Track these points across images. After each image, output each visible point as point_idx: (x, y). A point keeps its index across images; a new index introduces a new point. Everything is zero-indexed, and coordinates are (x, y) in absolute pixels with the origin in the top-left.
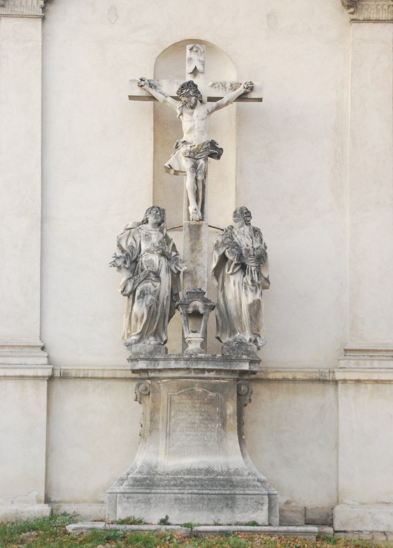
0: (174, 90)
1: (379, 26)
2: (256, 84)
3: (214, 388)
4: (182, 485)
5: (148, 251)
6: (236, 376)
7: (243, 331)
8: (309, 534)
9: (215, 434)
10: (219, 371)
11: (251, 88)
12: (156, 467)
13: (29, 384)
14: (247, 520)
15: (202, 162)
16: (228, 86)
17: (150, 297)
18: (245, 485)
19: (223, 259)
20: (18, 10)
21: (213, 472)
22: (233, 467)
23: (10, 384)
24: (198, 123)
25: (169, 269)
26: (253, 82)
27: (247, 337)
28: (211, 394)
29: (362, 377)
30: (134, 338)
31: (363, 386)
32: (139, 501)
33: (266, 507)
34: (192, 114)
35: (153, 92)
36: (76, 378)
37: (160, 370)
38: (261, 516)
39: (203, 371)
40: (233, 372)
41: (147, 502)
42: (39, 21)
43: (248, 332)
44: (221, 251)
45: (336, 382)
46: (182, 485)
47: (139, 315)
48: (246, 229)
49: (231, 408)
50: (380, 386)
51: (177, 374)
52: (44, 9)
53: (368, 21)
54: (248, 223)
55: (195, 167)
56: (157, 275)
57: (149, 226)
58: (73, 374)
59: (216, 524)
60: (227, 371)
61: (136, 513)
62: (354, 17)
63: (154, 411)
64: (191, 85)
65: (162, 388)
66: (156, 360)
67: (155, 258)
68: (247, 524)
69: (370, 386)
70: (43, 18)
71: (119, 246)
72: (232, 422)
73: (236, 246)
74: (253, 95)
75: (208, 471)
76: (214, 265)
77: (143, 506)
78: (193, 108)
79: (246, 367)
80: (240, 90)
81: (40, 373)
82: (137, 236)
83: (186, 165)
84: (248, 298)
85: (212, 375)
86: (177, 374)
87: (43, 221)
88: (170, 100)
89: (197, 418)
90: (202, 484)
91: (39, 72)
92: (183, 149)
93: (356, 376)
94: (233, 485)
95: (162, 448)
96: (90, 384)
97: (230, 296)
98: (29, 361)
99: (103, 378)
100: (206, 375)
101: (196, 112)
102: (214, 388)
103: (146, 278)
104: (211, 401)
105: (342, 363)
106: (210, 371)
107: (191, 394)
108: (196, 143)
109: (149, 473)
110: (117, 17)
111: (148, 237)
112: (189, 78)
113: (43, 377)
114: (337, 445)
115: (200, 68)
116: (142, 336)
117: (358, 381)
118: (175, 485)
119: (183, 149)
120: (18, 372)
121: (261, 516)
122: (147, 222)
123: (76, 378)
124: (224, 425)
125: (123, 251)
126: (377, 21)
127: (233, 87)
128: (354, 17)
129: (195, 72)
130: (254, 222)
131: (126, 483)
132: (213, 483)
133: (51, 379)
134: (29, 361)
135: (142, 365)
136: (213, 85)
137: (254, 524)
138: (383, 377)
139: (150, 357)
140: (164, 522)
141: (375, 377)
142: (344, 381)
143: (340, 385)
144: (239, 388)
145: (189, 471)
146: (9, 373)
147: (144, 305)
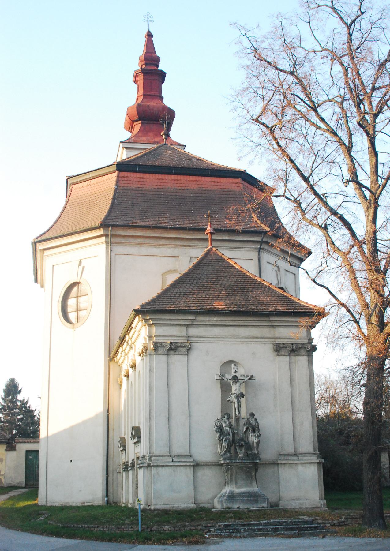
0: (230, 378)
1: (285, 357)
2: (254, 375)
3: (248, 468)
4: (243, 497)
5: (226, 426)
6: (255, 464)
7: (255, 450)
9: (250, 481)
10: (250, 463)
11: (252, 377)
12: (233, 492)
13: (188, 468)
14: (261, 506)
15: (240, 399)
16: (245, 376)
17: (228, 441)
18: (260, 496)
19: (247, 428)
20: (180, 353)
21: (251, 493)
23: (182, 468)
24: (238, 388)
25: (232, 432)
27: (256, 452)
28: (248, 469)
29: (286, 462)
30: (223, 453)
31: (286, 465)
32: (230, 502)
33: (266, 502)
34: (236, 385)
35: (224, 378)
36: (202, 465)
37: (233, 463)
38: (265, 505)
39: (246, 463)
40: (254, 463)
41: (233, 502)
42: (186, 356)
43: (256, 450)
44: (247, 426)
45: (278, 464)
46: (243, 497)
47: (225, 446)
48: (253, 419)
49: (253, 474)
50: (291, 465)
51: (238, 464)
52: (187, 352)
53: (282, 355)
54: (254, 417)
55: (238, 400)
57: (225, 419)
58: (200, 464)
59: (253, 508)
60: (252, 462)
62: (278, 354)
63: (231, 475)
64: (235, 376)
65: (233, 468)
66: (232, 460)
67: (228, 429)
68: (262, 507)
69: (288, 465)
70: (187, 355)
71: (216, 425)
72: (254, 477)
73: (251, 424)
74: (253, 379)
75: (249, 492)
76: (244, 430)
77: (231, 503)
78: (236, 383)
80: (249, 377)
81: (191, 464)
82: (222, 422)
83: (236, 400)
84: (255, 441)
85: (248, 464)
86: (238, 464)
87: (189, 416)
88: (229, 380)
89: (244, 477)
90: (248, 496)
91: (187, 371)
92: (233, 395)
93: (284, 462)
94: (257, 496)
95: (234, 486)
96: (205, 467)
97: (250, 440)
98: (188, 460)
99: (209, 465)
100: (247, 464)
101: (237, 384)
102: (248, 468)
103: (226, 435)
104: (248, 472)
105: (280, 458)
106: (247, 463)
108: (238, 394)
109: (231, 494)
110: (208, 354)
111: (225, 422)
112: (234, 374)
113: (192, 465)
114: (279, 482)
115: (237, 370)
116: (225, 452)
117: (285, 464)
118: (240, 497)
119: (233, 395)
120: (185, 464)
121: (265, 505)
122: (224, 417)
123: (202, 465)
125: (217, 426)
126: (284, 355)
127: (247, 376)
128: (278, 354)
129: (235, 372)
130: (255, 417)
131: (225, 497)
132: (251, 496)
133: (195, 466)
134: (188, 460)
135: (227, 461)
136: (241, 376)
137: (263, 507)
138: (292, 462)
139: (230, 458)
140: (238, 508)
141: (290, 462)
142: (281, 464)
143: (280, 466)
144: (255, 468)
145: (244, 493)
146: (182, 464)
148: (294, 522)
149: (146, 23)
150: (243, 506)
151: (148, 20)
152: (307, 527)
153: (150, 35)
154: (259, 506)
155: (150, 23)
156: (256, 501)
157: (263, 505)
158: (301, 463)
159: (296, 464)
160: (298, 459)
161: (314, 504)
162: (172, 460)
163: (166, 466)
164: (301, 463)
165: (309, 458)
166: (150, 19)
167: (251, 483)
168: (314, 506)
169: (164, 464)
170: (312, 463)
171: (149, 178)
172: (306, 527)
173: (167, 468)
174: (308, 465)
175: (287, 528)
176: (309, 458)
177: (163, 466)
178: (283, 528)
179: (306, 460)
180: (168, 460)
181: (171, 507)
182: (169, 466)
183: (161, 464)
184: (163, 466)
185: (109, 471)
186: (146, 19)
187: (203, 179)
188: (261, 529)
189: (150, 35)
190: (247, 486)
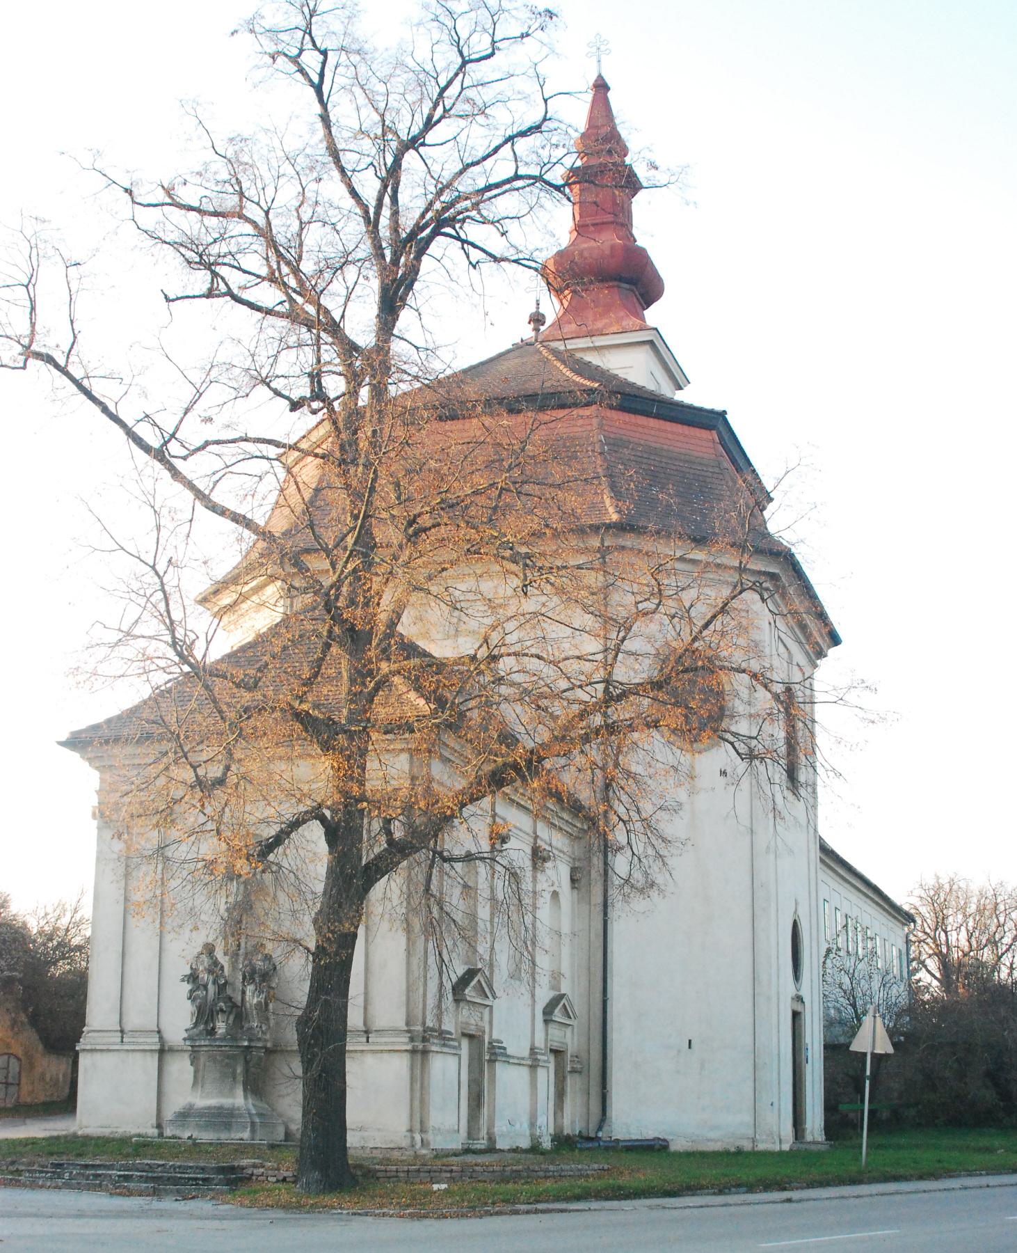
8: (565, 1183)
13: (148, 1054)
14: (237, 1137)
22: (236, 1105)
23: (138, 1055)
26: (833, 652)
36: (177, 1051)
39: (221, 1046)
41: (183, 1126)
56: (205, 987)
58: (175, 1048)
61: (178, 1133)
75: (220, 1108)
79: (246, 1044)
81: (154, 1047)
85: (227, 1049)
90: (213, 1115)
98: (148, 1040)
102: (228, 1057)
107: (215, 1060)
120: (141, 1047)
123: (177, 1051)
124: (234, 1079)
134: (148, 1040)
137: (242, 1139)
144: (245, 1058)
147: (917, 902)
148: (180, 1167)
149: (595, 59)
150: (205, 1136)
151: (599, 49)
152: (189, 1179)
153: (601, 87)
154: (233, 1136)
155: (603, 58)
156: (228, 1126)
157: (240, 1135)
158: (373, 1051)
159: (362, 1051)
160: (368, 1041)
161: (392, 1141)
162: (119, 1040)
163: (109, 1050)
164: (373, 1051)
165: (392, 1040)
166: (603, 48)
167: (232, 1090)
168: (392, 1146)
169: (104, 1047)
170: (394, 1051)
171: (673, 433)
172: (185, 1178)
173: (111, 1054)
174: (386, 1056)
175: (147, 1177)
176: (392, 1040)
177: (102, 1051)
178: (141, 1177)
179: (381, 1044)
180: (112, 1040)
181: (112, 1133)
182: (114, 1050)
183: (98, 1047)
184: (102, 1051)
185: (599, 1099)
186: (594, 49)
187: (641, 420)
188: (100, 1175)
189: (601, 87)
190: (221, 1094)
